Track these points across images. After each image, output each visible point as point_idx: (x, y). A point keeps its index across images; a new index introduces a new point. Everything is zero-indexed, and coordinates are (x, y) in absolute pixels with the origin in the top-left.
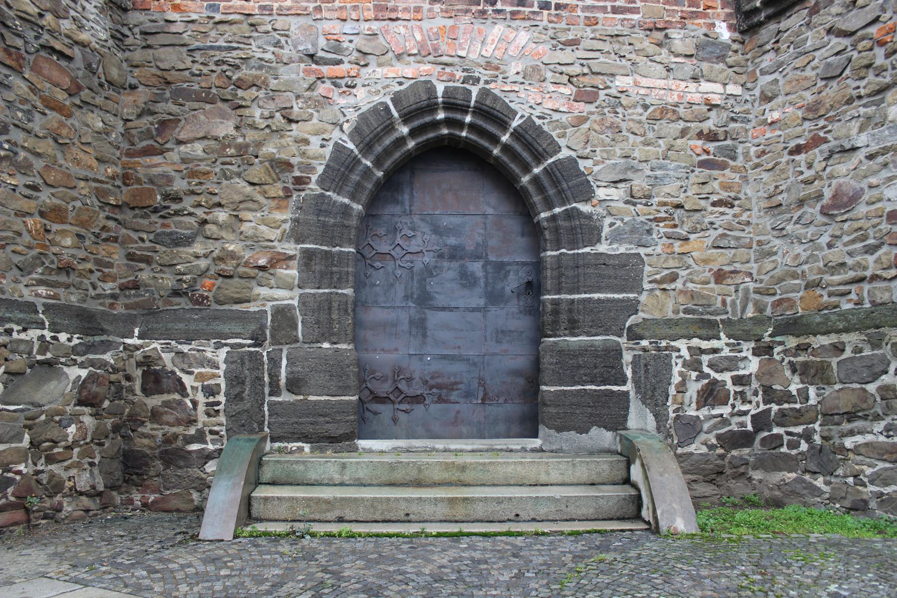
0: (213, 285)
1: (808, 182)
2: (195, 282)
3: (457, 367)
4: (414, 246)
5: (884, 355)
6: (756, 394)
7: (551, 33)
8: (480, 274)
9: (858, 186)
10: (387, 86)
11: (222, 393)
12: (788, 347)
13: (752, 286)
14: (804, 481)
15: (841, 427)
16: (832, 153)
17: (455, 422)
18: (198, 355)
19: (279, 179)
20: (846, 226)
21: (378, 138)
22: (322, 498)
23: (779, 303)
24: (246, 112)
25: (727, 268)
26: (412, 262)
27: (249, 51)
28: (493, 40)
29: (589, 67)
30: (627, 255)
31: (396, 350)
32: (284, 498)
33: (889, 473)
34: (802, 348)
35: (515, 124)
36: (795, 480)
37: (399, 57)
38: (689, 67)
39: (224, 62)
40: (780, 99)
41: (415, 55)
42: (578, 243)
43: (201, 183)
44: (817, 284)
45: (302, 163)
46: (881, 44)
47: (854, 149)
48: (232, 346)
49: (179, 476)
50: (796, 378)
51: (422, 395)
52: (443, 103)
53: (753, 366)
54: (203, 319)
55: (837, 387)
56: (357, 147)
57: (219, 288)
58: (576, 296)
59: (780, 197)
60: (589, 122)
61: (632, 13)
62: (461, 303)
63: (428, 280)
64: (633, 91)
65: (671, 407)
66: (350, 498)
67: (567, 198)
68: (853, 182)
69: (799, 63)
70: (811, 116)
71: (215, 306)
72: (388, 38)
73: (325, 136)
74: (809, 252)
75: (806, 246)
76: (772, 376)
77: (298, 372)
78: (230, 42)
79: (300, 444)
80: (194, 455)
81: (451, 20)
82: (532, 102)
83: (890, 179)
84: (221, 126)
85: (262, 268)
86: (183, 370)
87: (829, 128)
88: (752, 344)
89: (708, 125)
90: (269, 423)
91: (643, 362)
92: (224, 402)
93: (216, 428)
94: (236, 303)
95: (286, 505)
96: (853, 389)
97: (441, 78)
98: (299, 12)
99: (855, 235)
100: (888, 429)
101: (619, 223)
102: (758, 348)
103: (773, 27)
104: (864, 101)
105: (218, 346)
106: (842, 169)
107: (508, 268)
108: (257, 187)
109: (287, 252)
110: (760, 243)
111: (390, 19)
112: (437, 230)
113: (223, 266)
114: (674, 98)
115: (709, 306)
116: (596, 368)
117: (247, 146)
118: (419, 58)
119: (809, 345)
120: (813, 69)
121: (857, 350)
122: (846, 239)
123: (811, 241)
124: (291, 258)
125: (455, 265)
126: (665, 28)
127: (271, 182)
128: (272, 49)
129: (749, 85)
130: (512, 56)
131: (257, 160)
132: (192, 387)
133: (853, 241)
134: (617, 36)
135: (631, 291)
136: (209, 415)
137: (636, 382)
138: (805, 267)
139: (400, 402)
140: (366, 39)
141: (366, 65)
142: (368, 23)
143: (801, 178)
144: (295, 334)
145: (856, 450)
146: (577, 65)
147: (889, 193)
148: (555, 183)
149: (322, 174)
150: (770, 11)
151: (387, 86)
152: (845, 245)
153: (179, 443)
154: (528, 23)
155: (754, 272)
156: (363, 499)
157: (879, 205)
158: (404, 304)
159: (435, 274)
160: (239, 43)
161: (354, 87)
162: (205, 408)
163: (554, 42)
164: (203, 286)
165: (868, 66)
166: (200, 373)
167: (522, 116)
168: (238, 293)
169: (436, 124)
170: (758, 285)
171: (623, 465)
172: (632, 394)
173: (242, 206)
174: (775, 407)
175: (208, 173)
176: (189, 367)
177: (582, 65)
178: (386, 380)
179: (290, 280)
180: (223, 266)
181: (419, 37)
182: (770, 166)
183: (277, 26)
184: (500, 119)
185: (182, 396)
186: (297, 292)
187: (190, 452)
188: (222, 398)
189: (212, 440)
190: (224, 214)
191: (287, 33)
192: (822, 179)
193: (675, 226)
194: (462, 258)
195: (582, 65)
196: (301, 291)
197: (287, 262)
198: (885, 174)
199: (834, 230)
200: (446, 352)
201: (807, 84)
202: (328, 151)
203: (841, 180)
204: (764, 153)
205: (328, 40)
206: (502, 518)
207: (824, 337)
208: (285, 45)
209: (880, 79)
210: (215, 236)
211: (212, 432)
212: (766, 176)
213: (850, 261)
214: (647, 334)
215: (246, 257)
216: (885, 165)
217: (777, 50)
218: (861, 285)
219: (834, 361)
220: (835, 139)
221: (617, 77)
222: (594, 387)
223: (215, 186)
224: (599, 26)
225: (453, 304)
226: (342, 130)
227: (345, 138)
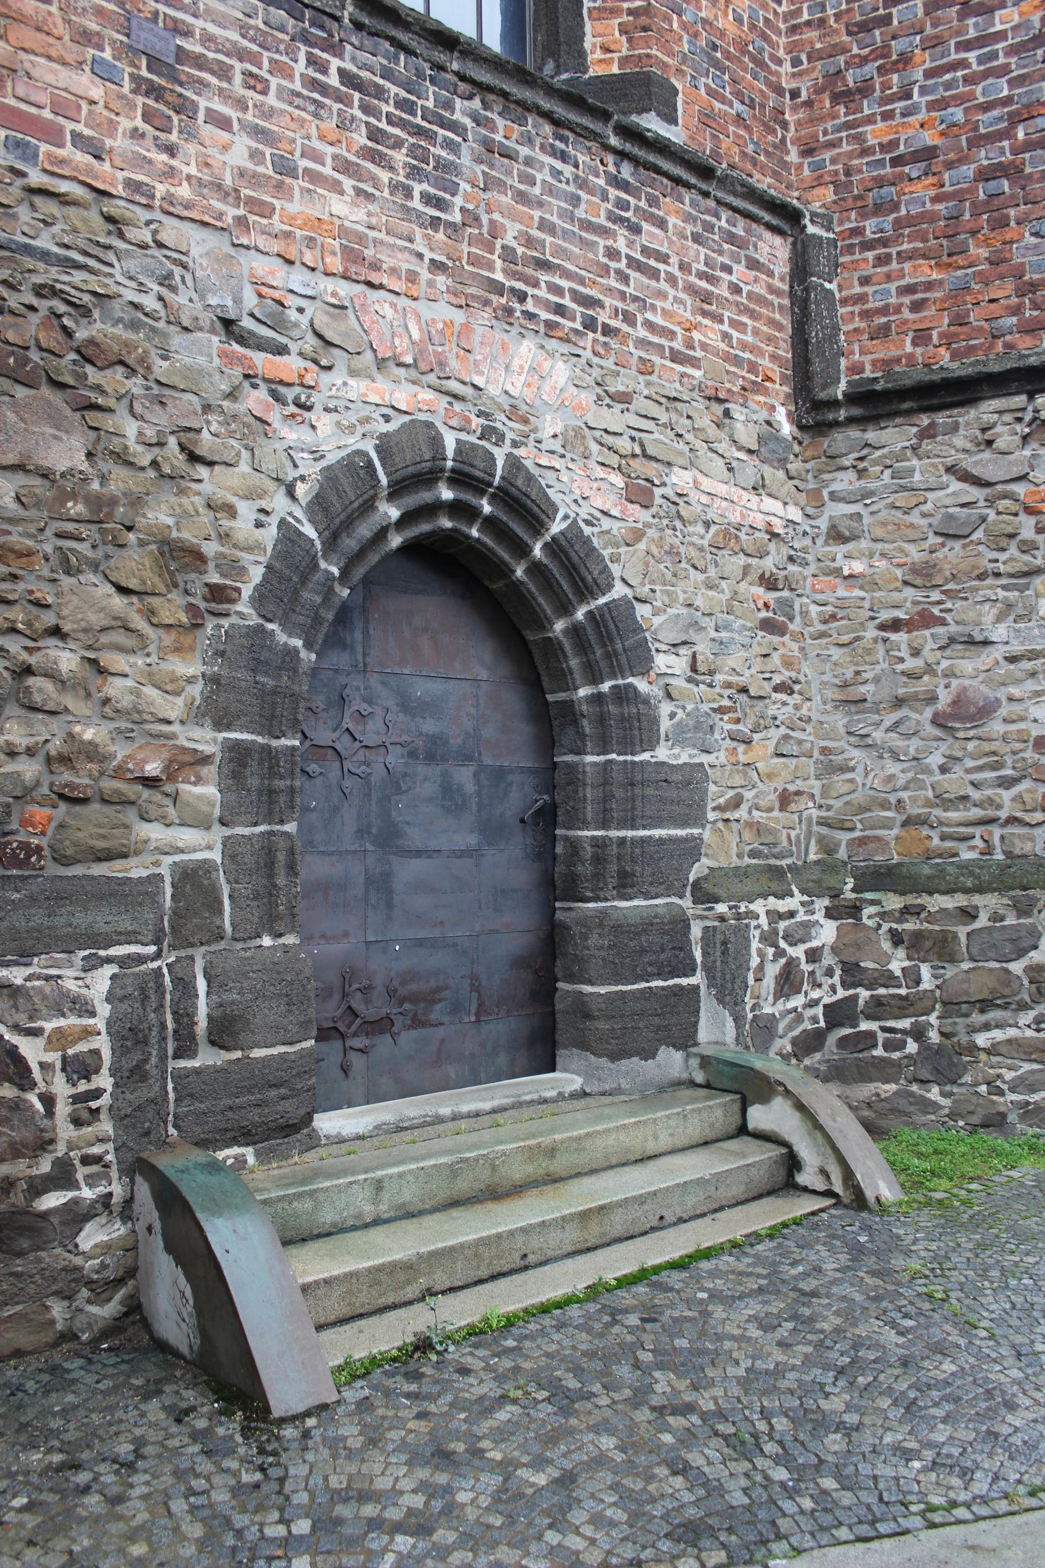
0: (50, 819)
1: (913, 676)
2: (9, 814)
3: (436, 960)
4: (372, 732)
5: (1033, 925)
6: (829, 973)
7: (596, 372)
8: (470, 788)
9: (991, 695)
10: (367, 420)
11: (105, 1071)
12: (887, 909)
13: (815, 813)
14: (912, 1094)
15: (969, 1020)
16: (952, 640)
17: (439, 1059)
18: (47, 990)
19: (176, 585)
20: (971, 746)
21: (349, 523)
22: (400, 1261)
23: (862, 841)
24: (108, 422)
25: (792, 788)
26: (368, 765)
27: (109, 281)
28: (521, 367)
29: (642, 446)
30: (691, 765)
31: (346, 935)
32: (336, 1278)
33: (1037, 1077)
34: (907, 911)
35: (556, 527)
36: (896, 1093)
37: (381, 363)
38: (750, 469)
39: (55, 293)
40: (864, 544)
41: (407, 366)
42: (633, 744)
43: (14, 577)
44: (921, 821)
45: (223, 556)
46: (1030, 511)
47: (986, 643)
48: (123, 962)
49: (17, 1275)
50: (901, 953)
51: (388, 1017)
52: (453, 470)
53: (827, 933)
54: (32, 899)
55: (966, 966)
56: (320, 534)
57: (61, 826)
58: (630, 834)
59: (863, 689)
60: (644, 540)
61: (693, 366)
62: (440, 842)
63: (394, 798)
64: (694, 496)
65: (749, 1001)
66: (443, 1249)
67: (620, 666)
68: (982, 688)
69: (900, 498)
70: (918, 582)
71: (54, 870)
72: (366, 319)
73: (263, 504)
74: (911, 775)
75: (906, 765)
76: (859, 948)
77: (233, 1003)
78: (67, 247)
79: (236, 1150)
80: (55, 1220)
81: (461, 312)
82: (578, 492)
83: (1038, 694)
84: (56, 447)
85: (150, 782)
86: (17, 1028)
87: (949, 605)
88: (826, 902)
89: (768, 564)
90: (176, 1116)
91: (719, 937)
92: (110, 1089)
93: (96, 1150)
94: (99, 860)
95: (338, 1291)
96: (991, 970)
97: (451, 423)
98: (207, 219)
99: (985, 760)
100: (1038, 1021)
101: (680, 715)
102: (835, 907)
103: (854, 433)
104: (1004, 581)
105: (92, 964)
106: (967, 666)
107: (510, 778)
108: (135, 599)
109: (200, 747)
110: (825, 751)
111: (370, 284)
112: (407, 706)
113: (67, 776)
114: (735, 518)
115: (775, 845)
116: (663, 950)
117: (113, 502)
118: (413, 373)
119: (923, 908)
120: (924, 515)
121: (996, 917)
122: (970, 763)
123: (915, 759)
124: (205, 760)
125: (434, 771)
126: (726, 401)
127: (164, 591)
128: (156, 288)
129: (810, 511)
130: (546, 403)
131: (132, 537)
132: (42, 1065)
133: (981, 769)
134: (675, 399)
135: (694, 825)
136: (77, 1122)
137: (708, 969)
138: (904, 795)
139: (355, 1035)
140: (328, 313)
141: (329, 368)
142: (330, 279)
143: (900, 667)
144: (218, 922)
145: (992, 1051)
146: (626, 437)
147: (1035, 712)
148: (606, 638)
149: (261, 585)
150: (856, 411)
151: (367, 420)
152: (968, 771)
153: (18, 1198)
154: (566, 348)
155: (817, 792)
156: (462, 1246)
157: (1022, 726)
158: (356, 847)
159: (404, 787)
160: (86, 254)
161: (309, 409)
162: (69, 1109)
163: (599, 390)
164: (25, 822)
165: (1012, 536)
166: (58, 1030)
167: (566, 517)
168: (104, 837)
169: (434, 508)
170: (823, 813)
171: (736, 1107)
172: (703, 989)
173: (104, 639)
174: (864, 994)
175: (29, 554)
176: (31, 1018)
177: (633, 439)
178: (330, 995)
179: (206, 808)
180: (67, 776)
181: (416, 335)
182: (845, 639)
183: (162, 237)
184: (533, 515)
185: (22, 1088)
186: (219, 833)
187: (45, 1215)
188: (104, 1081)
189: (87, 1177)
190: (67, 654)
191: (184, 258)
192: (935, 675)
193: (738, 721)
194: (444, 759)
195: (633, 439)
196: (227, 832)
197: (198, 768)
198: (1030, 685)
199: (950, 747)
200: (421, 934)
201: (912, 534)
202: (270, 535)
203: (967, 682)
204: (833, 617)
205: (260, 295)
206: (643, 1229)
207: (945, 898)
208: (181, 286)
209: (1027, 558)
210: (51, 706)
211: (86, 1160)
212: (836, 653)
213: (975, 795)
214: (722, 893)
215: (119, 757)
216: (1033, 674)
217: (861, 473)
218: (989, 828)
219: (962, 931)
220: (957, 623)
221: (676, 469)
222: (660, 983)
223: (46, 587)
224: (654, 378)
225: (433, 845)
226: (291, 494)
227: (299, 513)
